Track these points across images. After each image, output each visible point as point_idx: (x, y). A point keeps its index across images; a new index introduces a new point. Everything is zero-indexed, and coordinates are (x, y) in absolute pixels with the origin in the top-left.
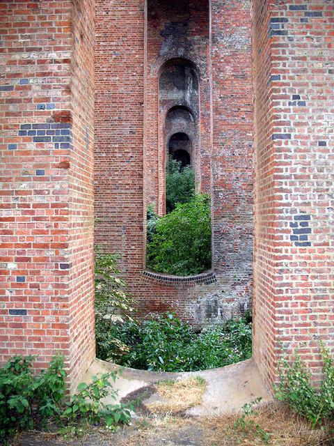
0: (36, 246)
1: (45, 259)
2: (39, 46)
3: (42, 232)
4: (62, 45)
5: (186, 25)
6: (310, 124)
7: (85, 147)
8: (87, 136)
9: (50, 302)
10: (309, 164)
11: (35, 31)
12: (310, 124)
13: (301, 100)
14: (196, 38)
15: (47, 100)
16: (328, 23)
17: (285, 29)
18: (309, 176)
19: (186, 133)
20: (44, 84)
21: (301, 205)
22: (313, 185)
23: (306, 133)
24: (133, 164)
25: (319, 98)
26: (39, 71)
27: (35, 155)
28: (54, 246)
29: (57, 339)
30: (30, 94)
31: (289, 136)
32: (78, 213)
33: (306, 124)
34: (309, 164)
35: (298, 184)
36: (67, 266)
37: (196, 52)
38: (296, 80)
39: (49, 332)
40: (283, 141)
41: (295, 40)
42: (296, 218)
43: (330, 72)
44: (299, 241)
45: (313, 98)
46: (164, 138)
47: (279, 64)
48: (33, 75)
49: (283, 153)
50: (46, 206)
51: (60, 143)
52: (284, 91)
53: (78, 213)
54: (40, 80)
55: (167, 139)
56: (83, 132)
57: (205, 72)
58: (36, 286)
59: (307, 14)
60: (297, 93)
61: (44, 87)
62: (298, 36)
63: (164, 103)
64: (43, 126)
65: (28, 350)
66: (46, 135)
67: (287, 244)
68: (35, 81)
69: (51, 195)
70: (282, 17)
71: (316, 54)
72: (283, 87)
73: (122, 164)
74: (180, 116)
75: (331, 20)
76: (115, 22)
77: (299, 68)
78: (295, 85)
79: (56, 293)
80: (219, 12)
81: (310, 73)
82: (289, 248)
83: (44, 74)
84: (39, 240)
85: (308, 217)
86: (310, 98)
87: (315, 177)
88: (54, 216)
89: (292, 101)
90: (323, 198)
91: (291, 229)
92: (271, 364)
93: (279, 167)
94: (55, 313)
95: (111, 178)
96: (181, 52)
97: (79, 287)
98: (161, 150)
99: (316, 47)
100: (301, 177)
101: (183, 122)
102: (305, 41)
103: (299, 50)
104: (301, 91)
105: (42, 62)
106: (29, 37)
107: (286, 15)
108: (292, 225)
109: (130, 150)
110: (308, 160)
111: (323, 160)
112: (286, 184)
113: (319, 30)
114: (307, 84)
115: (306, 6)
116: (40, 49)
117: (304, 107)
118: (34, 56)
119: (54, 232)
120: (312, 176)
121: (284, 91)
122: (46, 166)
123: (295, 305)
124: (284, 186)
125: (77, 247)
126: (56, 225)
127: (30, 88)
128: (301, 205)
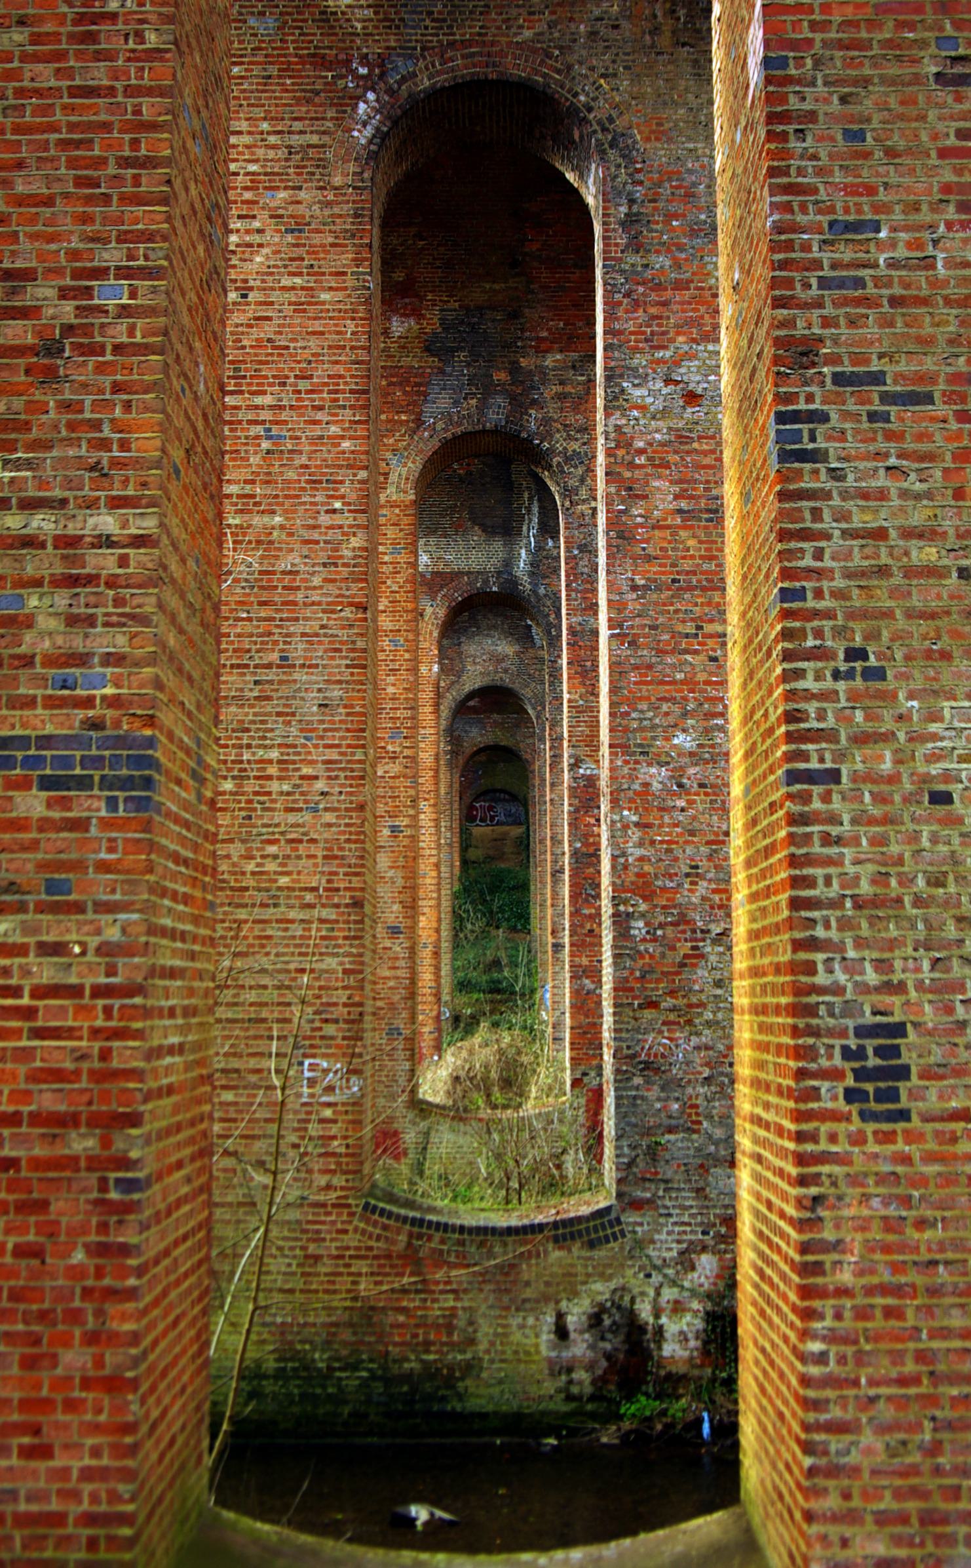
0: (36, 1119)
1: (71, 1162)
2: (58, 493)
3: (58, 1075)
4: (130, 492)
5: (515, 315)
6: (901, 736)
7: (191, 797)
8: (200, 761)
9: (77, 1303)
10: (900, 861)
11: (46, 445)
12: (901, 736)
13: (873, 661)
14: (551, 360)
15: (81, 659)
16: (954, 426)
17: (821, 444)
18: (899, 900)
19: (516, 686)
20: (75, 610)
21: (878, 990)
22: (914, 927)
23: (887, 766)
24: (329, 817)
25: (929, 655)
26: (59, 570)
27: (41, 830)
28: (95, 1121)
29: (96, 1428)
30: (29, 642)
31: (834, 776)
32: (172, 1013)
33: (889, 737)
34: (900, 861)
35: (864, 924)
36: (130, 1185)
37: (552, 410)
38: (857, 601)
39: (72, 1406)
40: (817, 790)
41: (851, 477)
42: (861, 1032)
43: (963, 573)
44: (873, 1106)
45: (908, 658)
46: (437, 705)
47: (802, 550)
48: (37, 583)
49: (815, 828)
50: (75, 991)
51: (120, 794)
52: (819, 634)
53: (172, 1013)
54: (61, 599)
55: (445, 712)
56: (188, 752)
57: (582, 480)
58: (35, 1252)
59: (886, 398)
60: (858, 641)
61: (72, 620)
62: (862, 465)
63: (435, 582)
64: (68, 741)
65: (586, 1253)
66: (78, 771)
67: (835, 1116)
68: (47, 601)
69: (91, 957)
70: (812, 407)
71: (918, 517)
72: (816, 623)
73: (292, 818)
74: (495, 627)
75: (962, 416)
76: (268, 330)
77: (866, 563)
78: (851, 615)
79: (100, 1273)
80: (627, 295)
81: (897, 579)
82: (841, 1128)
83: (73, 581)
84: (48, 1100)
85: (898, 1030)
86: (899, 656)
87: (918, 902)
88: (99, 1023)
89: (843, 667)
90: (948, 970)
91: (847, 1066)
92: (798, 1515)
93: (805, 872)
94: (92, 1338)
95: (251, 866)
96: (496, 414)
97: (166, 1253)
98: (426, 757)
99: (918, 497)
100: (875, 902)
101: (506, 648)
102: (882, 481)
103: (863, 509)
104: (872, 636)
105: (67, 542)
106: (28, 464)
107: (823, 403)
108: (847, 1054)
109: (320, 770)
110: (894, 849)
111: (943, 849)
112: (827, 926)
113: (924, 447)
114: (888, 614)
115: (883, 373)
116: (64, 502)
117: (879, 685)
118: (42, 523)
119: (99, 1076)
120: (907, 900)
121: (819, 634)
122: (78, 866)
123: (862, 1314)
124: (820, 932)
125: (164, 1123)
126: (105, 1055)
127: (29, 622)
128: (878, 990)
